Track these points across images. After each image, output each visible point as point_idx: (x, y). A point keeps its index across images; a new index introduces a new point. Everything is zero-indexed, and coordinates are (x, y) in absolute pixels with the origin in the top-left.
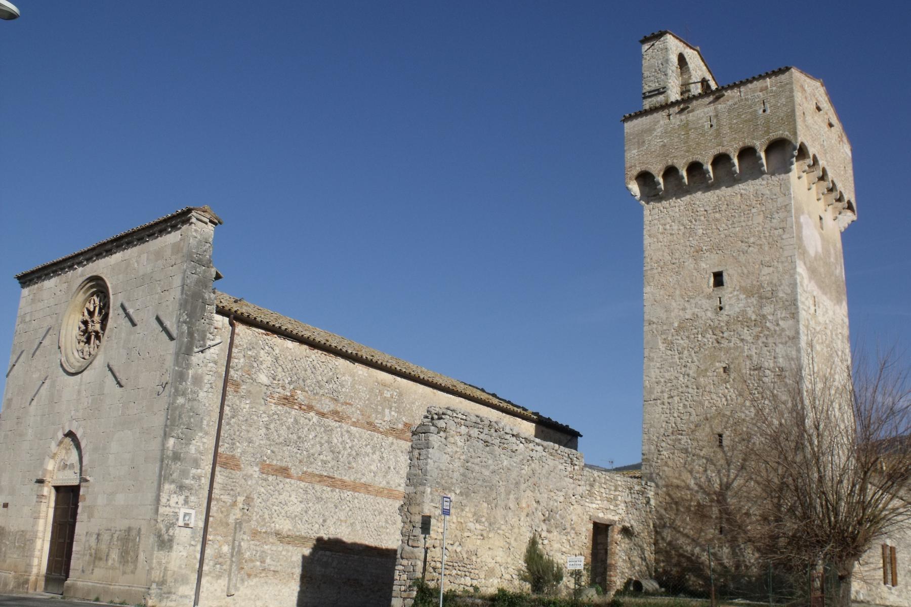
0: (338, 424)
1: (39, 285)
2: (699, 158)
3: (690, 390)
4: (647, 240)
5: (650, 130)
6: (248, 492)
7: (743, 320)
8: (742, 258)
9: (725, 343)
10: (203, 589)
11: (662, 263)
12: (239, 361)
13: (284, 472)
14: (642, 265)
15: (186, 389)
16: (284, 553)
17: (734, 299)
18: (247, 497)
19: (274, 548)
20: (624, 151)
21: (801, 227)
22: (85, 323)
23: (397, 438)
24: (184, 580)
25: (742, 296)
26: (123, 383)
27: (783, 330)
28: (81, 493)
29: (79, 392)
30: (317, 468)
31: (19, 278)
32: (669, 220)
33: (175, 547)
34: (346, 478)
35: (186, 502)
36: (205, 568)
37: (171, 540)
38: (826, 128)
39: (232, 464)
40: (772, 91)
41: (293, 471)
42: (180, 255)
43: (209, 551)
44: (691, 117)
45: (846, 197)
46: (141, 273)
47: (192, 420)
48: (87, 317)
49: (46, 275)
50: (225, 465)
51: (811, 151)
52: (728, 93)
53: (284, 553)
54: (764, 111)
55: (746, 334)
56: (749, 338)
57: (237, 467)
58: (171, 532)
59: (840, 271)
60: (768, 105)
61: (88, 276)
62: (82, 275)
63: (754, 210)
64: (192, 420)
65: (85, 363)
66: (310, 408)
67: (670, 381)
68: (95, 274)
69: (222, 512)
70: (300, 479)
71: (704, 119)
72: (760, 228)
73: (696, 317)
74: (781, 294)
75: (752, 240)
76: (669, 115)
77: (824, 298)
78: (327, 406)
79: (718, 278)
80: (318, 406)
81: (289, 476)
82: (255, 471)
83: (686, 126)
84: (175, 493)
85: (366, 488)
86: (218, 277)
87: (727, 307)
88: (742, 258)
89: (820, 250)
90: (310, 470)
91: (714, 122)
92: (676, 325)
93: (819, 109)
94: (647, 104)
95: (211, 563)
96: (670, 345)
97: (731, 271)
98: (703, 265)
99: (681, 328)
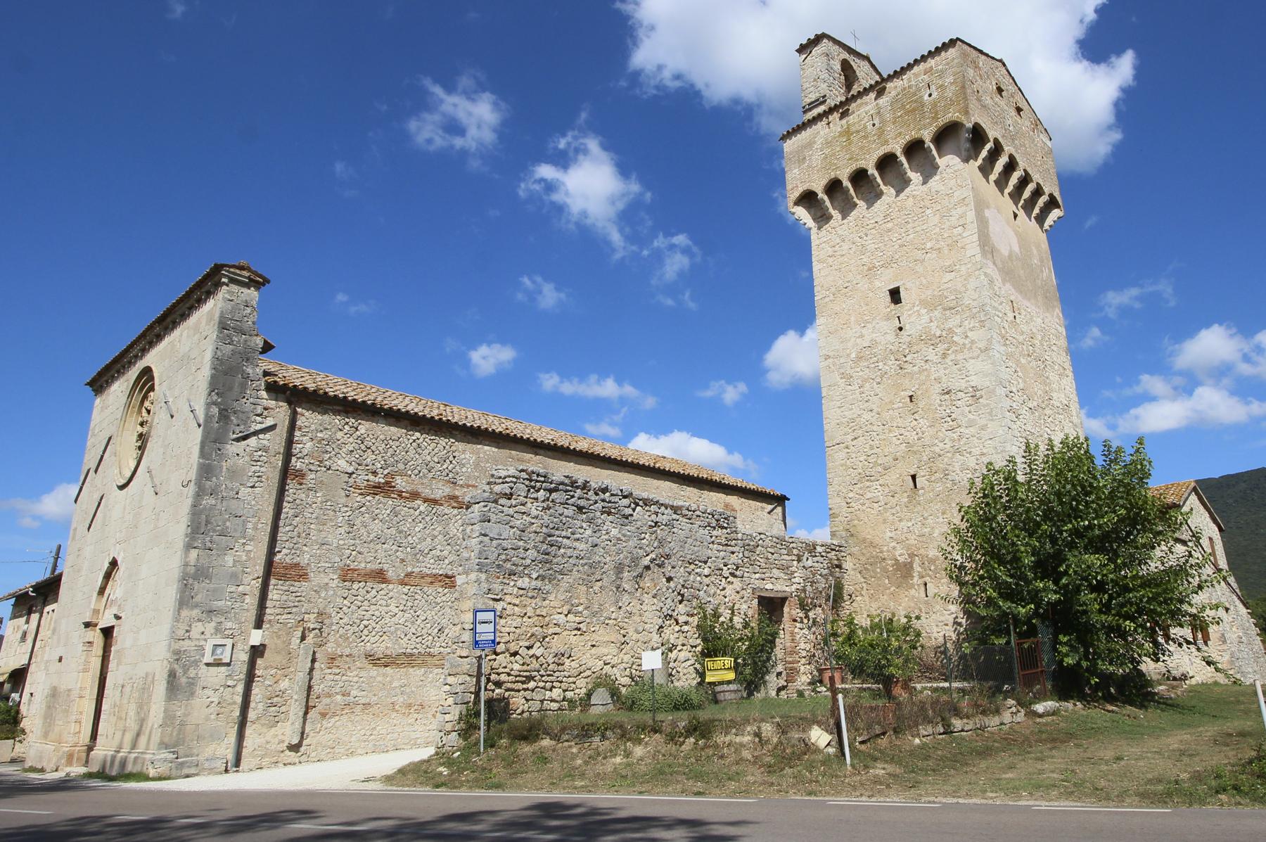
2: (862, 164)
3: (875, 428)
4: (816, 267)
5: (810, 145)
6: (321, 606)
7: (931, 340)
8: (919, 268)
9: (909, 368)
10: (248, 742)
11: (833, 289)
13: (380, 576)
17: (915, 316)
18: (320, 614)
19: (363, 674)
21: (987, 222)
24: (216, 737)
25: (924, 311)
27: (973, 342)
32: (838, 240)
33: (199, 691)
35: (218, 630)
36: (252, 715)
37: (192, 683)
38: (1014, 113)
39: (297, 573)
41: (390, 574)
43: (256, 691)
44: (851, 119)
45: (1047, 190)
47: (228, 524)
49: (118, 372)
50: (284, 577)
51: (992, 134)
52: (889, 85)
53: (379, 679)
56: (935, 358)
58: (192, 673)
59: (1048, 274)
60: (933, 87)
63: (928, 212)
64: (228, 524)
66: (415, 495)
67: (853, 420)
69: (279, 637)
70: (403, 583)
73: (874, 344)
75: (929, 245)
77: (1026, 303)
79: (895, 295)
80: (426, 492)
82: (333, 580)
83: (847, 133)
84: (199, 620)
87: (907, 327)
88: (919, 268)
89: (1016, 248)
92: (853, 355)
93: (1000, 90)
95: (261, 706)
96: (848, 378)
97: (909, 285)
98: (878, 284)
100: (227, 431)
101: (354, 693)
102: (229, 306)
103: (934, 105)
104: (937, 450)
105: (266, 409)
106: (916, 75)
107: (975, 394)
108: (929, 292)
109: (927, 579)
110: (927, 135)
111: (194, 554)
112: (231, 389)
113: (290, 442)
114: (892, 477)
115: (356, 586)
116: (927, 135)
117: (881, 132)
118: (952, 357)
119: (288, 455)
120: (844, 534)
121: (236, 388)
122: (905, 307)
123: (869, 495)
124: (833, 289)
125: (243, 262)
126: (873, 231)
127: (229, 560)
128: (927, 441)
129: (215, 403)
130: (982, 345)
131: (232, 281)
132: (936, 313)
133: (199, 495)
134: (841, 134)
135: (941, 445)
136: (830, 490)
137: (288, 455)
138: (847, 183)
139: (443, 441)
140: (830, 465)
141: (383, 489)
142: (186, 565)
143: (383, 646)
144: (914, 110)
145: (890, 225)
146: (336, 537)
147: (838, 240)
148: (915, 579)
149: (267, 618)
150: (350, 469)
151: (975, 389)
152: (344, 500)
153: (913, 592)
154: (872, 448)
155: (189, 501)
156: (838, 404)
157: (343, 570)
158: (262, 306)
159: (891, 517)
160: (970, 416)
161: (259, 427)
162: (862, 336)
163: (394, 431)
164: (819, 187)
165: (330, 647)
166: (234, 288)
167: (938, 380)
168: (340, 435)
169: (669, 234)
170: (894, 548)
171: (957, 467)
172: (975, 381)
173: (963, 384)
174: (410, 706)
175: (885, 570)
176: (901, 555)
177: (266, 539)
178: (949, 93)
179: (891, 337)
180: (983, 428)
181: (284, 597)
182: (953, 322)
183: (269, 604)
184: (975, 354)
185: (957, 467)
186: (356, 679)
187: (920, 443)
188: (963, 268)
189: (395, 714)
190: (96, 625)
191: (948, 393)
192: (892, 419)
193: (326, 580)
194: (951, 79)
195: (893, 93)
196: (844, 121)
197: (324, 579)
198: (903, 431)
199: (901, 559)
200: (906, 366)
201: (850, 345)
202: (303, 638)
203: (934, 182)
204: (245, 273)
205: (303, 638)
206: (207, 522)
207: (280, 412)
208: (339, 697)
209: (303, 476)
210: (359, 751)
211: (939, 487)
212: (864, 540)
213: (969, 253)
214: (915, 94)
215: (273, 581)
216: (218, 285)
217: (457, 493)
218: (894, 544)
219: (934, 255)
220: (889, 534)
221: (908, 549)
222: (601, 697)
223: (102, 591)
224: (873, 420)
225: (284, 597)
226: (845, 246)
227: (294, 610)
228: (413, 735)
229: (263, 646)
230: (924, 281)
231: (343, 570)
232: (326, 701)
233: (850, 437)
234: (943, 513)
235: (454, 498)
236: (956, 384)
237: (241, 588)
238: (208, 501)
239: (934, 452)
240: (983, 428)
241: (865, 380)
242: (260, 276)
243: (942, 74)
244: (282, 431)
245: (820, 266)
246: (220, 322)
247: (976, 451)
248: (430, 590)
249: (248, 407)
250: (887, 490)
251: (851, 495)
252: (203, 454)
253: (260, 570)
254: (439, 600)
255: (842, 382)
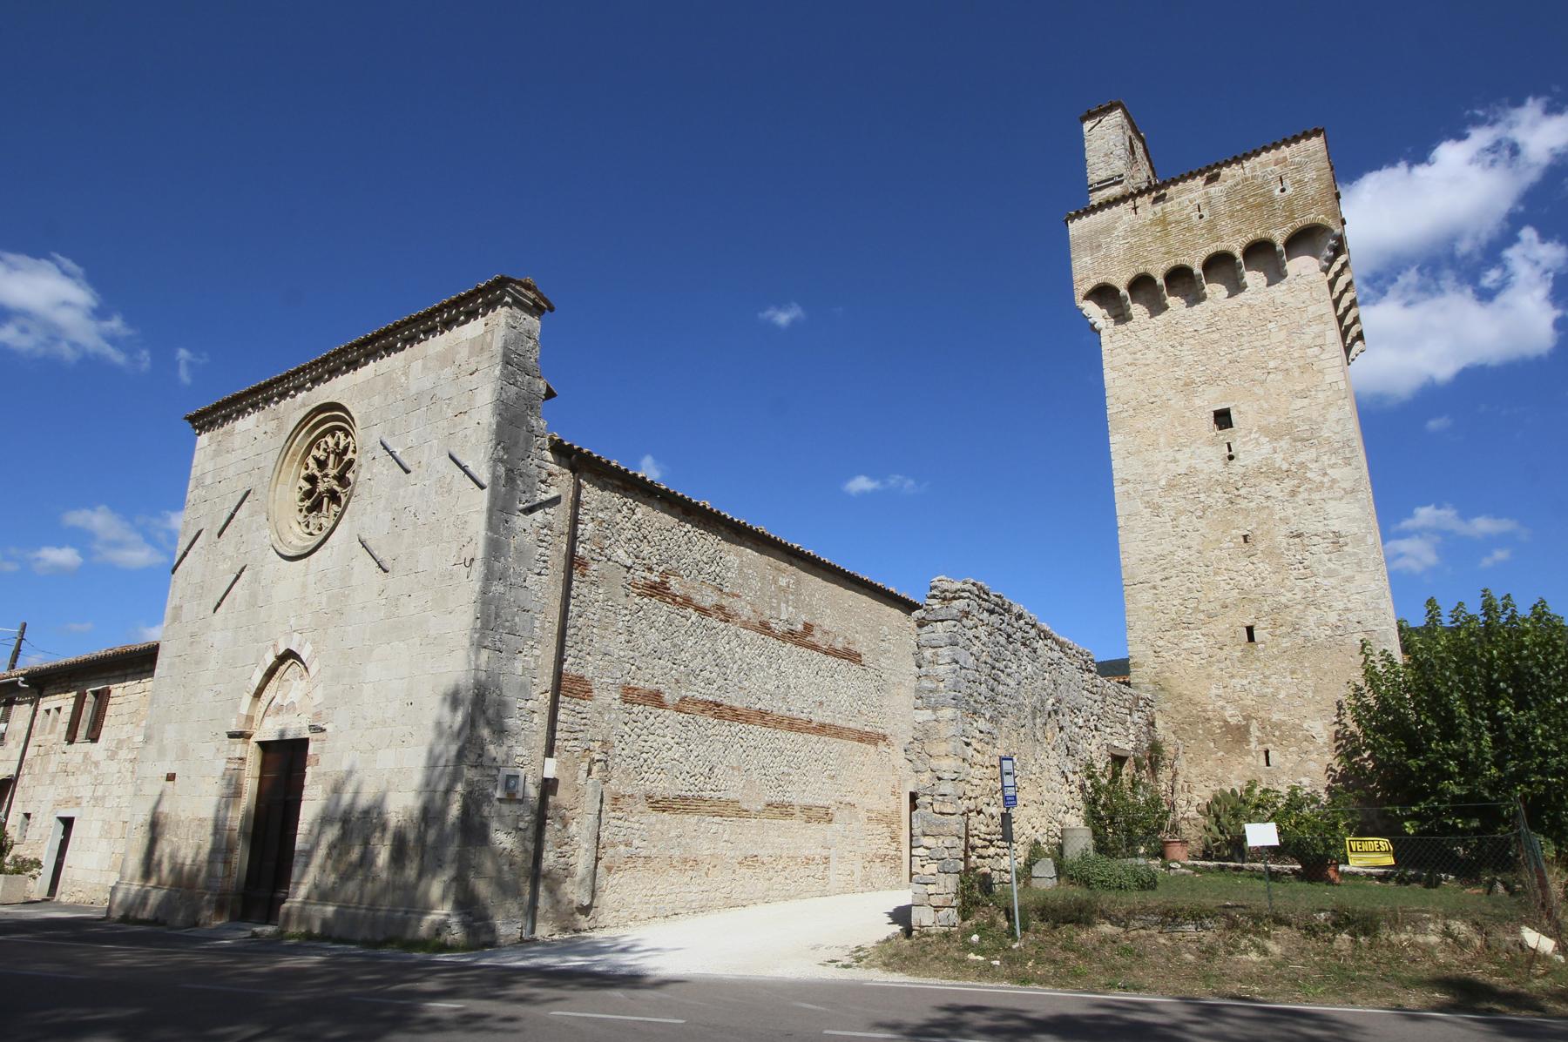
0: (723, 625)
1: (227, 427)
2: (1184, 260)
3: (1194, 568)
4: (1108, 375)
5: (1108, 230)
7: (1268, 471)
8: (1259, 390)
12: (587, 528)
13: (656, 699)
14: (1103, 407)
15: (506, 569)
16: (658, 826)
17: (1251, 445)
20: (1069, 260)
22: (312, 479)
23: (797, 644)
25: (1264, 440)
26: (386, 566)
27: (1334, 481)
28: (311, 751)
29: (304, 586)
30: (700, 691)
31: (192, 419)
32: (1140, 347)
34: (736, 705)
39: (581, 688)
40: (1292, 163)
41: (667, 697)
42: (486, 355)
46: (413, 391)
48: (313, 468)
50: (571, 694)
54: (1283, 190)
55: (1274, 489)
57: (587, 694)
60: (1287, 182)
61: (314, 405)
62: (304, 405)
65: (313, 542)
67: (1163, 557)
68: (335, 400)
71: (1190, 209)
72: (1284, 348)
74: (1326, 434)
75: (1272, 364)
76: (1135, 208)
78: (709, 599)
79: (1223, 419)
80: (697, 598)
81: (662, 705)
82: (612, 698)
83: (1163, 222)
85: (763, 716)
86: (550, 394)
87: (1241, 456)
90: (690, 694)
91: (1205, 212)
92: (1163, 483)
94: (1096, 198)
96: (1157, 510)
97: (1243, 408)
98: (1198, 402)
99: (1171, 486)
100: (514, 499)
101: (636, 843)
102: (512, 334)
103: (1290, 201)
104: (1283, 600)
105: (550, 475)
106: (1263, 165)
107: (1337, 541)
108: (1273, 419)
109: (1270, 746)
110: (1279, 237)
111: (485, 654)
112: (516, 444)
113: (575, 521)
114: (1220, 627)
115: (636, 709)
116: (1279, 237)
117: (1212, 227)
118: (1305, 495)
119: (573, 538)
120: (1151, 687)
121: (522, 444)
122: (1238, 435)
123: (1186, 645)
124: (1134, 403)
125: (529, 280)
126: (1191, 341)
127: (518, 666)
128: (1269, 588)
129: (501, 460)
130: (1348, 485)
131: (517, 303)
132: (1282, 443)
133: (489, 577)
134: (1153, 223)
135: (1289, 595)
136: (1130, 635)
137: (573, 538)
138: (1160, 281)
139: (711, 537)
140: (1129, 606)
141: (658, 590)
142: (477, 669)
143: (662, 786)
144: (1260, 205)
145: (1216, 336)
146: (617, 646)
147: (1140, 347)
148: (1253, 746)
149: (557, 743)
150: (629, 563)
151: (1337, 534)
152: (623, 600)
153: (1249, 759)
154: (1190, 590)
155: (477, 586)
156: (1141, 537)
157: (623, 687)
158: (545, 339)
159: (1218, 673)
160: (1330, 565)
161: (545, 497)
162: (1175, 461)
163: (668, 520)
164: (1121, 282)
165: (613, 785)
166: (517, 311)
167: (1285, 520)
168: (619, 516)
169: (176, 365)
170: (1223, 708)
171: (1311, 621)
172: (1336, 525)
173: (1321, 528)
174: (685, 861)
175: (1210, 732)
176: (1233, 715)
177: (554, 642)
178: (1311, 190)
179: (1218, 465)
180: (1349, 579)
181: (571, 719)
182: (1306, 455)
183: (559, 726)
184: (1338, 495)
185: (1311, 621)
186: (637, 826)
187: (1258, 590)
188: (1320, 395)
189: (672, 871)
190: (249, 737)
191: (1298, 536)
192: (1220, 560)
193: (609, 700)
194: (1314, 175)
195: (1230, 182)
196: (1158, 208)
197: (608, 697)
198: (1234, 575)
199: (1233, 721)
200: (1239, 500)
201: (1158, 469)
202: (589, 772)
203: (1279, 290)
204: (531, 295)
205: (589, 772)
206: (497, 616)
207: (562, 483)
208: (622, 847)
209: (586, 565)
210: (642, 916)
211: (1286, 643)
212: (1180, 696)
213: (1328, 379)
214: (1261, 187)
215: (561, 698)
216: (498, 302)
217: (724, 603)
218: (1221, 703)
219: (1280, 376)
220: (1214, 691)
221: (1242, 710)
222: (1045, 871)
223: (258, 693)
224: (1191, 559)
225: (571, 719)
226: (1151, 355)
227: (580, 735)
228: (689, 897)
229: (555, 781)
230: (1266, 406)
231: (623, 687)
232: (611, 851)
233: (1158, 576)
234: (1293, 672)
235: (721, 608)
236: (1311, 526)
237: (529, 704)
238: (497, 588)
239: (1278, 602)
240: (1349, 579)
241: (1181, 513)
242: (545, 301)
243: (1300, 167)
244: (565, 508)
245: (1115, 375)
246: (504, 355)
247: (1339, 605)
248: (701, 719)
249: (534, 470)
250: (1212, 641)
251: (1160, 643)
252: (491, 526)
253: (547, 681)
254: (709, 733)
255: (1146, 513)
